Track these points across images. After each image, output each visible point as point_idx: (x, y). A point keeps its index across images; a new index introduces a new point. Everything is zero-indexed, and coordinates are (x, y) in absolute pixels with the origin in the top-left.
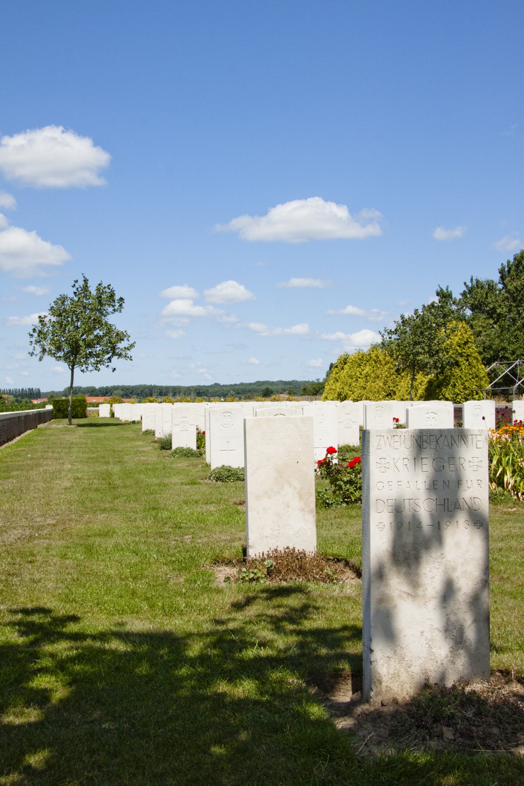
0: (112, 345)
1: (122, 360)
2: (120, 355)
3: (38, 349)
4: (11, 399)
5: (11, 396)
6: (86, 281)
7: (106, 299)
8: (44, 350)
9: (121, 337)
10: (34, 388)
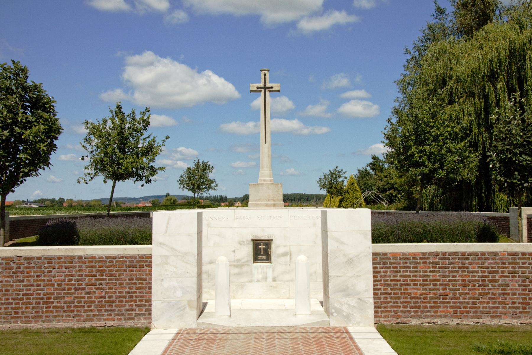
0: (209, 184)
1: (213, 191)
2: (212, 189)
3: (182, 186)
6: (198, 160)
7: (206, 167)
8: (184, 187)
9: (213, 182)
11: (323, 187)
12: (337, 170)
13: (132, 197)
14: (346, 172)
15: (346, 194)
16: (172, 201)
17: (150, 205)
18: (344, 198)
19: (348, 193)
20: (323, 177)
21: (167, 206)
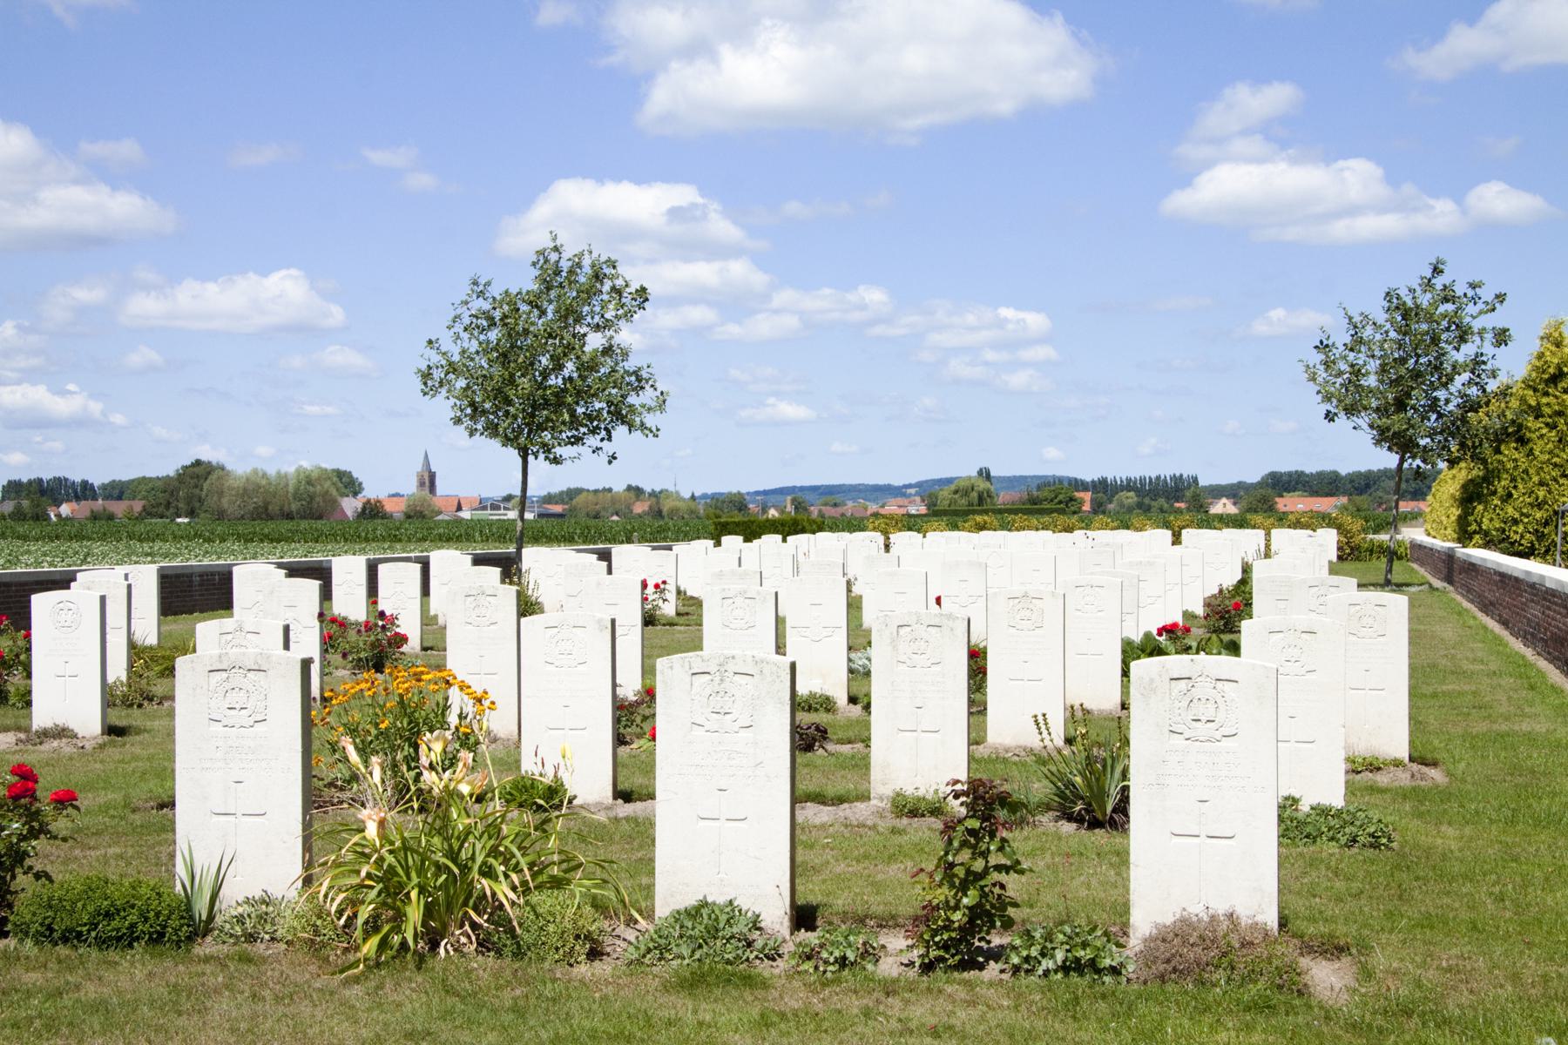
11: (1347, 400)
12: (1439, 282)
13: (881, 482)
14: (1501, 298)
15: (1509, 450)
16: (975, 495)
17: (923, 510)
18: (1490, 477)
19: (1522, 441)
20: (1341, 338)
21: (956, 513)
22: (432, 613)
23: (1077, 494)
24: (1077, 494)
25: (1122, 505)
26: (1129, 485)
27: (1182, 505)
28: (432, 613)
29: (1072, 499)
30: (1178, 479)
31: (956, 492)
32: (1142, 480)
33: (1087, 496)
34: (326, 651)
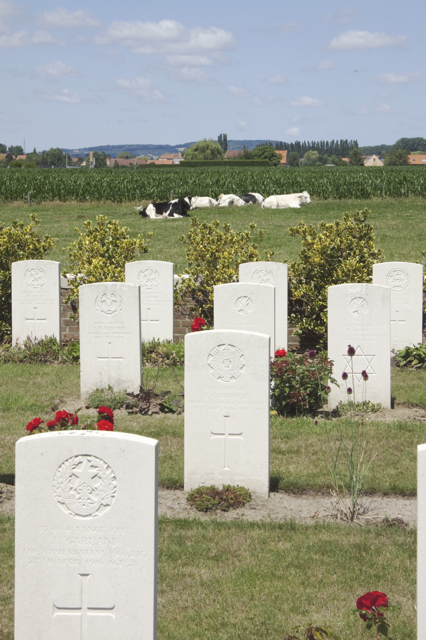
4: (314, 156)
5: (315, 152)
10: (349, 141)
13: (163, 143)
16: (209, 151)
22: (179, 163)
23: (277, 152)
24: (277, 152)
25: (309, 159)
26: (314, 147)
27: (346, 160)
28: (179, 163)
29: (273, 155)
30: (344, 143)
31: (196, 150)
32: (322, 143)
33: (284, 153)
34: (275, 438)
